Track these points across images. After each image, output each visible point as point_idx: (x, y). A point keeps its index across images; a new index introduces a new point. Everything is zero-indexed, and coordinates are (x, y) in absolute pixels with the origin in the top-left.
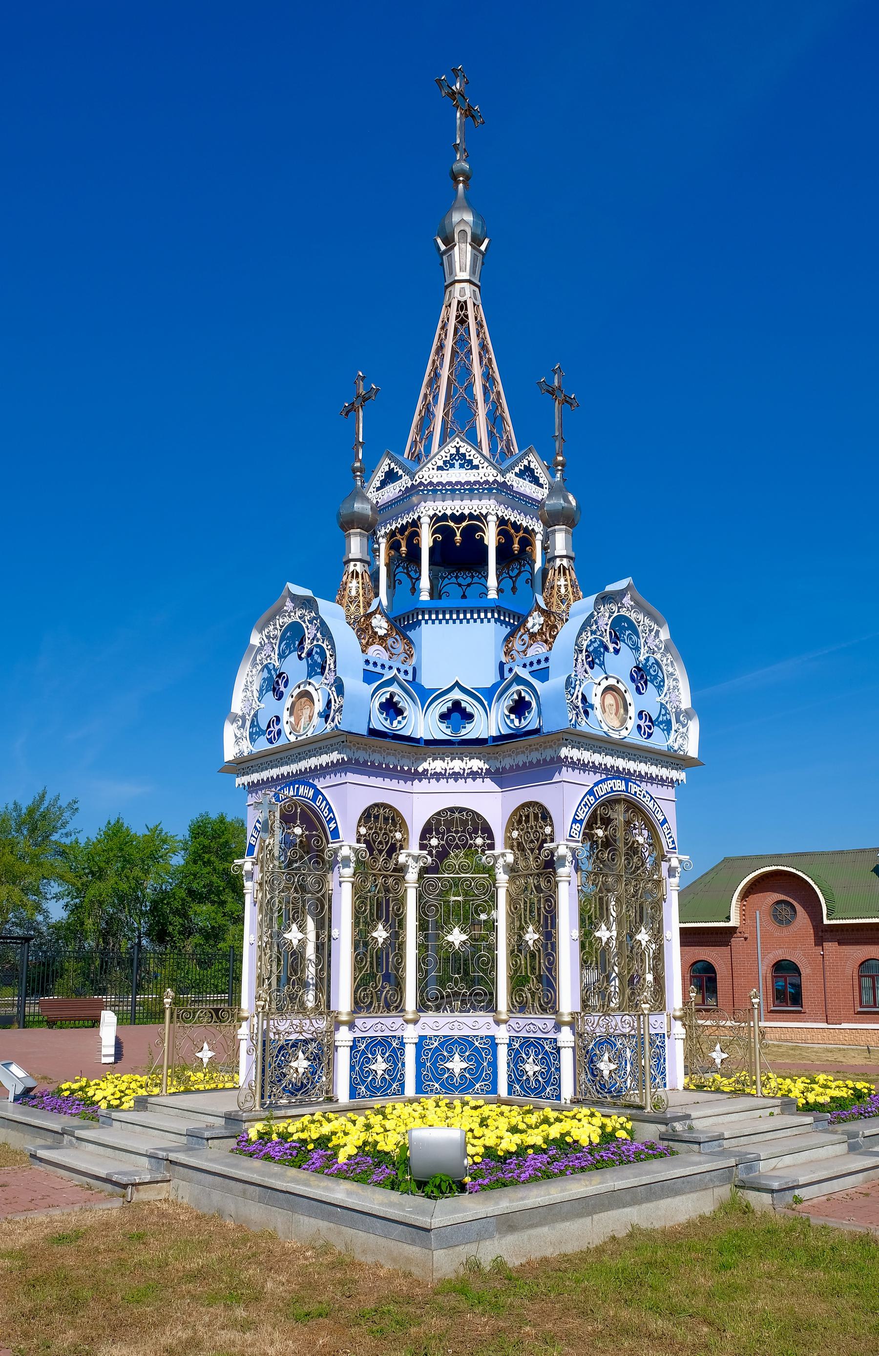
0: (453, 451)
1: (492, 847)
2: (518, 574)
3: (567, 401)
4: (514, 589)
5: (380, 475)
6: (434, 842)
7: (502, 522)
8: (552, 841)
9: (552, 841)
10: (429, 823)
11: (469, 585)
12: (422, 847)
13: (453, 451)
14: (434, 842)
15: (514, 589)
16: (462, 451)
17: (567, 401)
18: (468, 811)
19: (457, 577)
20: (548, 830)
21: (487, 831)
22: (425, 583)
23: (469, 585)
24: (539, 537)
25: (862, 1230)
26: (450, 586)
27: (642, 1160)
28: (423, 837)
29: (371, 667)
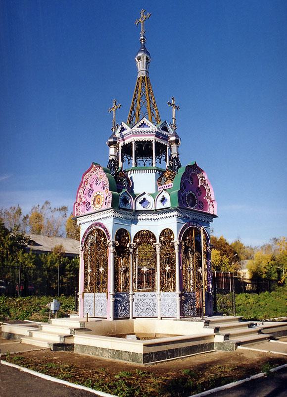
0: (142, 122)
1: (155, 242)
2: (161, 158)
3: (177, 108)
4: (160, 162)
5: (140, 123)
6: (138, 240)
7: (157, 143)
8: (173, 240)
9: (173, 240)
10: (136, 235)
11: (146, 161)
12: (134, 242)
13: (142, 122)
14: (138, 240)
15: (160, 162)
16: (145, 122)
17: (177, 108)
18: (149, 231)
19: (142, 158)
20: (172, 237)
21: (154, 237)
22: (133, 161)
23: (146, 161)
24: (168, 147)
25: (112, 253)
26: (140, 161)
27: (107, 265)
28: (134, 239)
29: (119, 188)
